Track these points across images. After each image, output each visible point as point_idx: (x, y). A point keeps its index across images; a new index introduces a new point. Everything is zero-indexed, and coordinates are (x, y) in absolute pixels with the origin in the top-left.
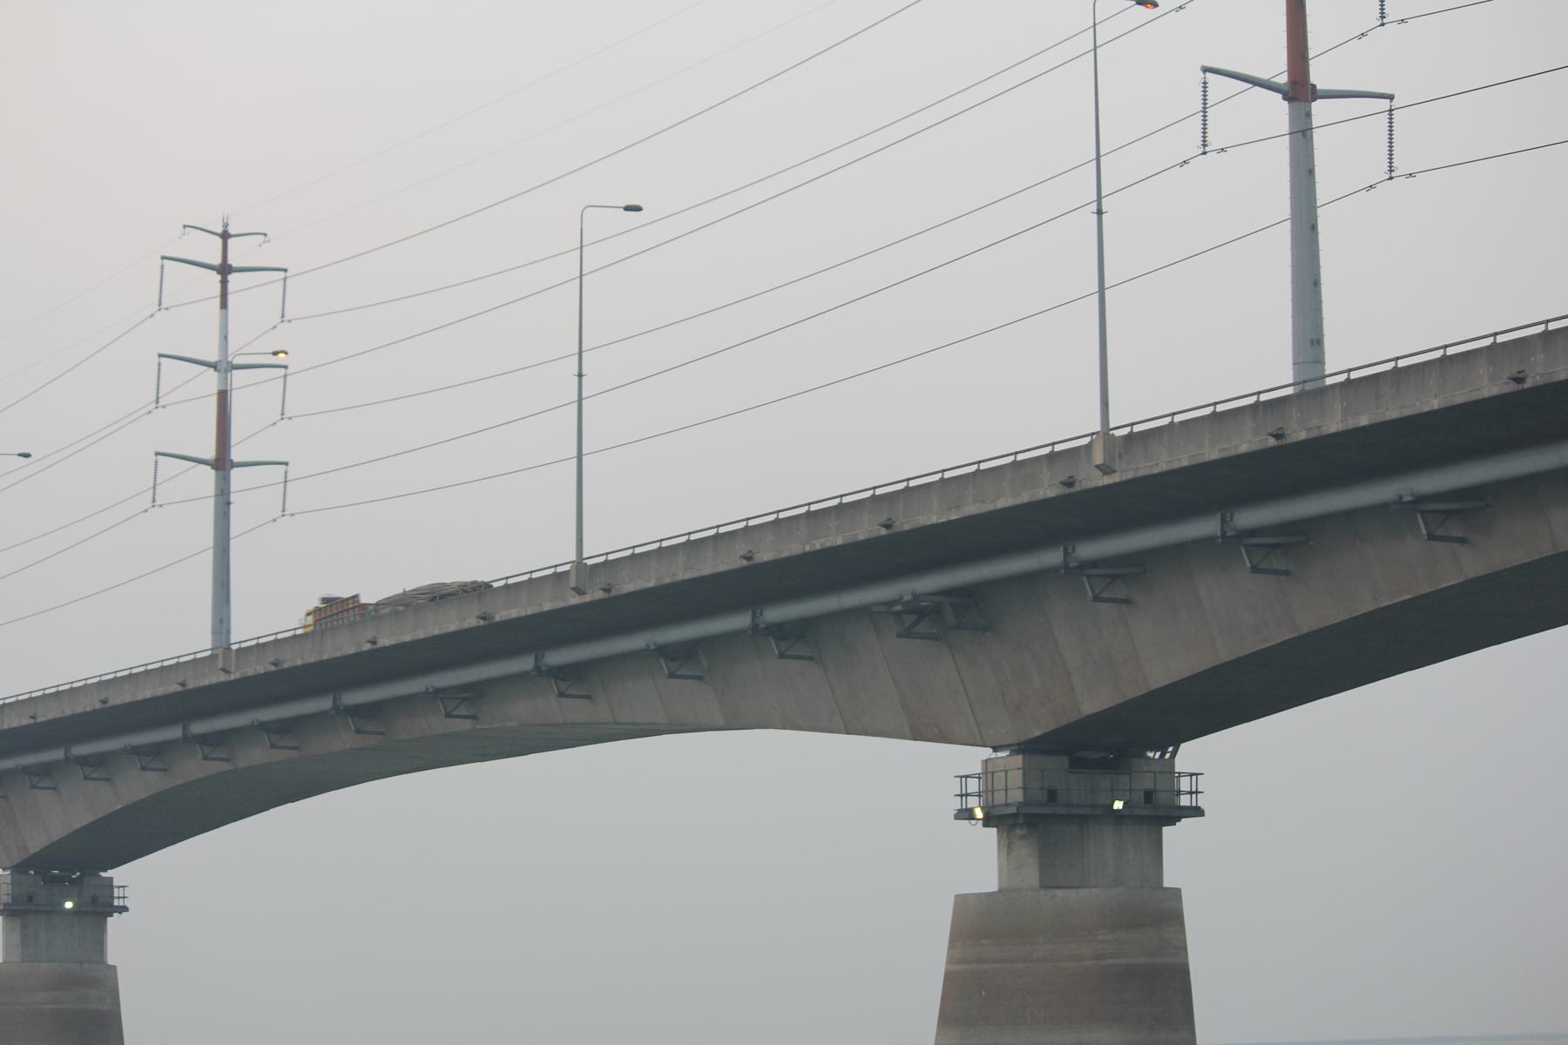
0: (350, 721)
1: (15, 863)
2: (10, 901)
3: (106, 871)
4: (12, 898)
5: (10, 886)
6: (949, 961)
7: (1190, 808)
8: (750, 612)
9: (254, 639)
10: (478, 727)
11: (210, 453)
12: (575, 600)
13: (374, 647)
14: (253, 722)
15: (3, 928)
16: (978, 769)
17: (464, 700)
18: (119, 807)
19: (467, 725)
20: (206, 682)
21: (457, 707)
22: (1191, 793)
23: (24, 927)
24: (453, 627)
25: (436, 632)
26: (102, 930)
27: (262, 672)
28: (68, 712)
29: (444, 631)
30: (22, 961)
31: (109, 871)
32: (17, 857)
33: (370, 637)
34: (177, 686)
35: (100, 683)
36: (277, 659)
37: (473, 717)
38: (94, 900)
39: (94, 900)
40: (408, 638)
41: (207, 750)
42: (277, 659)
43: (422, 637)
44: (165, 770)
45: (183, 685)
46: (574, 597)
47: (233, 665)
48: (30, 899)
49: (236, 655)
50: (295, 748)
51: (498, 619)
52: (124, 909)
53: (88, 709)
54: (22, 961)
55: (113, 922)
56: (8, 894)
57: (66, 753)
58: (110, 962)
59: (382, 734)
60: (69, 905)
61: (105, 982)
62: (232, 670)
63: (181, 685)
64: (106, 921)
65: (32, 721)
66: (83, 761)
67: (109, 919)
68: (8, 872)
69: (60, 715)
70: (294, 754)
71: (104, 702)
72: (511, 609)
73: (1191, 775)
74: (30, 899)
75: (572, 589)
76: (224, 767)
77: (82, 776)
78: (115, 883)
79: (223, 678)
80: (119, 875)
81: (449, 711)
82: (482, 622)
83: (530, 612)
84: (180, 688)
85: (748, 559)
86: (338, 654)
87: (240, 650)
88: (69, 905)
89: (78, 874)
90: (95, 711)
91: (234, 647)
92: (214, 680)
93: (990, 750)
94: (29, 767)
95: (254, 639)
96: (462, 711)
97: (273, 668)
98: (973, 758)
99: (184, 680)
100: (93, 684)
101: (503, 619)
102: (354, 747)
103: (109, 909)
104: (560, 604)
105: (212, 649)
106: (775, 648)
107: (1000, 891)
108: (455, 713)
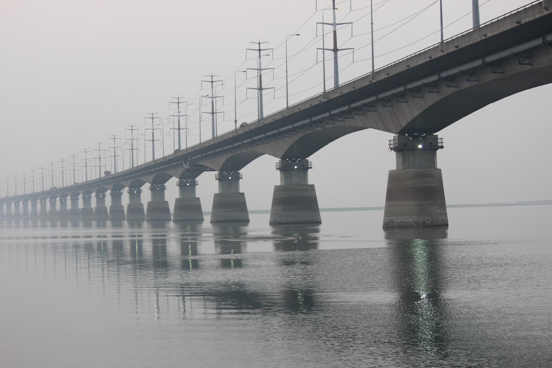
0: (464, 76)
1: (399, 131)
2: (397, 146)
3: (435, 133)
4: (398, 145)
5: (397, 140)
6: (388, 186)
7: (441, 146)
8: (542, 37)
9: (406, 57)
10: (533, 68)
11: (152, 140)
12: (546, 13)
13: (486, 37)
14: (422, 84)
15: (396, 157)
16: (393, 139)
17: (526, 57)
18: (427, 107)
19: (528, 67)
20: (437, 56)
21: (416, 94)
22: (441, 143)
23: (403, 156)
24: (509, 28)
25: (504, 30)
26: (434, 155)
27: (453, 51)
28: (398, 72)
29: (506, 29)
30: (403, 169)
31: (436, 133)
32: (399, 129)
33: (484, 34)
34: (429, 58)
35: (407, 59)
36: (457, 45)
37: (530, 64)
38: (431, 144)
39: (431, 144)
40: (496, 33)
41: (448, 83)
42: (457, 45)
43: (500, 32)
44: (438, 92)
45: (430, 58)
46: (545, 11)
47: (445, 49)
48: (405, 145)
49: (446, 44)
50: (477, 81)
51: (522, 23)
52: (442, 147)
53: (404, 70)
54: (403, 169)
55: (439, 152)
56: (396, 143)
57: (405, 88)
58: (438, 167)
59: (503, 73)
60: (420, 146)
61: (438, 176)
62: (445, 51)
63: (407, 66)
64: (436, 152)
65: (388, 76)
66: (412, 90)
67: (437, 151)
68: (397, 135)
69: (396, 73)
70: (477, 83)
71: (408, 66)
72: (526, 18)
73: (441, 139)
74: (405, 145)
75: (544, 8)
76: (455, 90)
77: (411, 96)
78: (439, 137)
79: (442, 54)
80: (440, 134)
81: (448, 85)
82: (518, 25)
83: (532, 18)
84: (430, 59)
85: (264, 123)
86: (475, 41)
87: (447, 42)
88: (420, 146)
89: (424, 134)
90: (406, 70)
91: (445, 42)
92: (439, 55)
93: (395, 134)
94: (427, 83)
95: (406, 57)
96: (526, 61)
97: (456, 49)
98: (394, 135)
99: (431, 56)
100: (397, 63)
101: (524, 22)
102: (495, 79)
103: (437, 147)
104: (541, 15)
105: (474, 28)
106: (490, 70)
107: (397, 169)
108: (523, 62)
